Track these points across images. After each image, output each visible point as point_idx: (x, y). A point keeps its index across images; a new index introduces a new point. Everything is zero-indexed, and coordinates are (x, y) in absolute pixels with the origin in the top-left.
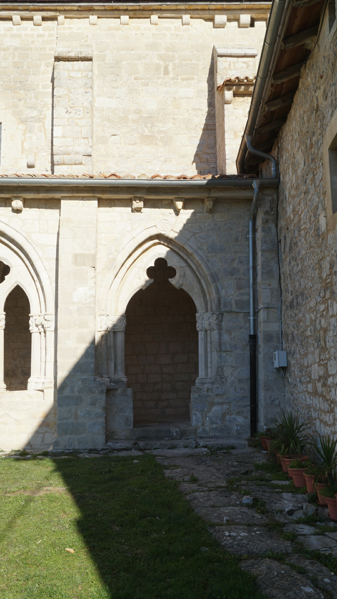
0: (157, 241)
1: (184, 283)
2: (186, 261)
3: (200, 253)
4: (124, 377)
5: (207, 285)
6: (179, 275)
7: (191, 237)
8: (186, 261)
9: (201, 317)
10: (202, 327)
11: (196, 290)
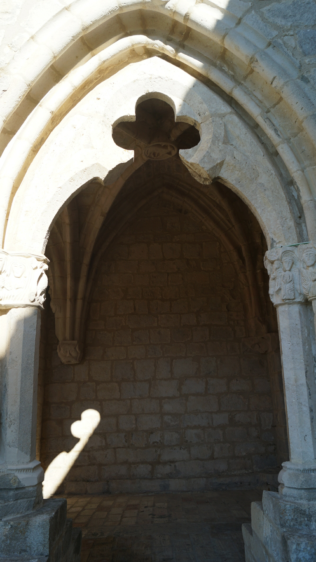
0: (141, 39)
1: (228, 158)
2: (230, 100)
3: (278, 58)
4: (27, 470)
5: (299, 160)
6: (211, 136)
7: (248, 11)
8: (230, 100)
9: (287, 259)
10: (294, 290)
11: (264, 179)
